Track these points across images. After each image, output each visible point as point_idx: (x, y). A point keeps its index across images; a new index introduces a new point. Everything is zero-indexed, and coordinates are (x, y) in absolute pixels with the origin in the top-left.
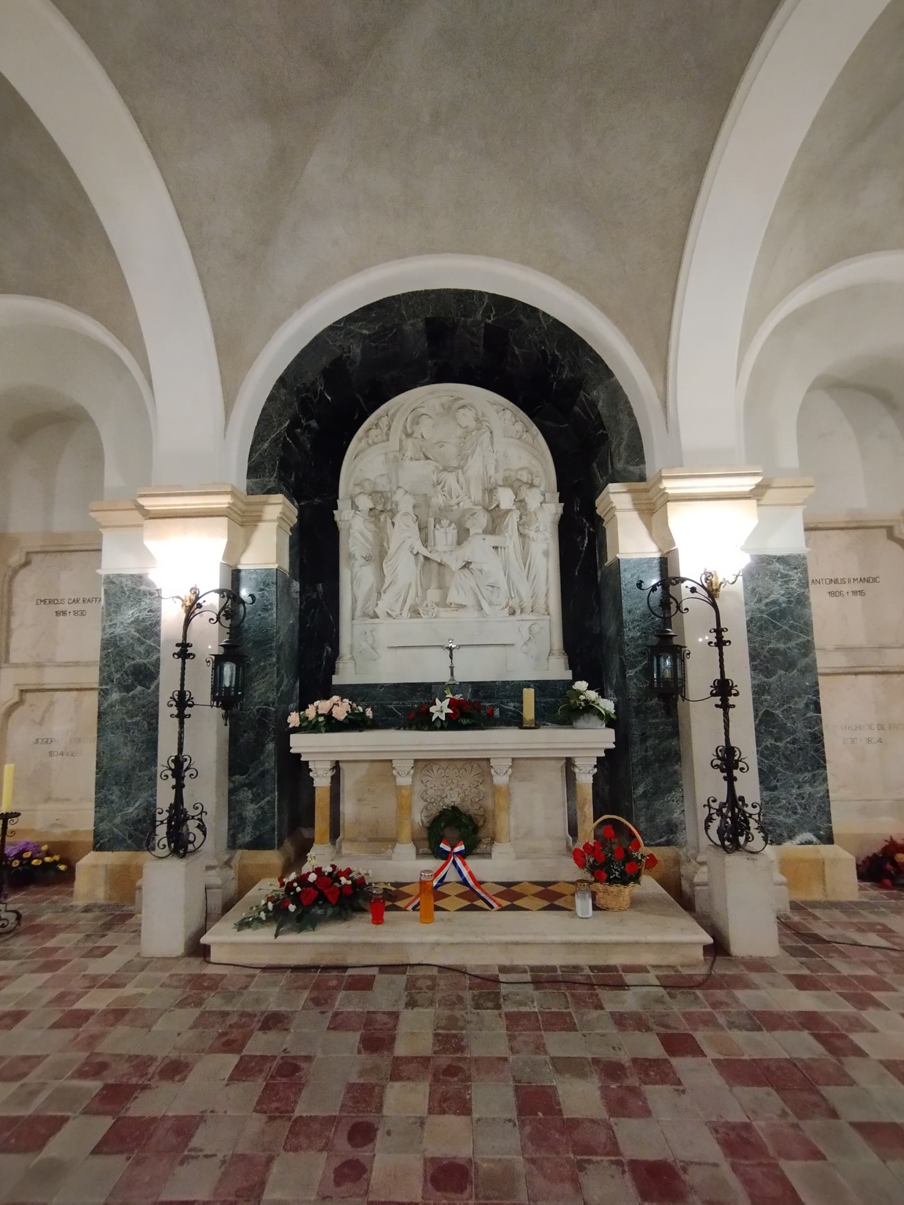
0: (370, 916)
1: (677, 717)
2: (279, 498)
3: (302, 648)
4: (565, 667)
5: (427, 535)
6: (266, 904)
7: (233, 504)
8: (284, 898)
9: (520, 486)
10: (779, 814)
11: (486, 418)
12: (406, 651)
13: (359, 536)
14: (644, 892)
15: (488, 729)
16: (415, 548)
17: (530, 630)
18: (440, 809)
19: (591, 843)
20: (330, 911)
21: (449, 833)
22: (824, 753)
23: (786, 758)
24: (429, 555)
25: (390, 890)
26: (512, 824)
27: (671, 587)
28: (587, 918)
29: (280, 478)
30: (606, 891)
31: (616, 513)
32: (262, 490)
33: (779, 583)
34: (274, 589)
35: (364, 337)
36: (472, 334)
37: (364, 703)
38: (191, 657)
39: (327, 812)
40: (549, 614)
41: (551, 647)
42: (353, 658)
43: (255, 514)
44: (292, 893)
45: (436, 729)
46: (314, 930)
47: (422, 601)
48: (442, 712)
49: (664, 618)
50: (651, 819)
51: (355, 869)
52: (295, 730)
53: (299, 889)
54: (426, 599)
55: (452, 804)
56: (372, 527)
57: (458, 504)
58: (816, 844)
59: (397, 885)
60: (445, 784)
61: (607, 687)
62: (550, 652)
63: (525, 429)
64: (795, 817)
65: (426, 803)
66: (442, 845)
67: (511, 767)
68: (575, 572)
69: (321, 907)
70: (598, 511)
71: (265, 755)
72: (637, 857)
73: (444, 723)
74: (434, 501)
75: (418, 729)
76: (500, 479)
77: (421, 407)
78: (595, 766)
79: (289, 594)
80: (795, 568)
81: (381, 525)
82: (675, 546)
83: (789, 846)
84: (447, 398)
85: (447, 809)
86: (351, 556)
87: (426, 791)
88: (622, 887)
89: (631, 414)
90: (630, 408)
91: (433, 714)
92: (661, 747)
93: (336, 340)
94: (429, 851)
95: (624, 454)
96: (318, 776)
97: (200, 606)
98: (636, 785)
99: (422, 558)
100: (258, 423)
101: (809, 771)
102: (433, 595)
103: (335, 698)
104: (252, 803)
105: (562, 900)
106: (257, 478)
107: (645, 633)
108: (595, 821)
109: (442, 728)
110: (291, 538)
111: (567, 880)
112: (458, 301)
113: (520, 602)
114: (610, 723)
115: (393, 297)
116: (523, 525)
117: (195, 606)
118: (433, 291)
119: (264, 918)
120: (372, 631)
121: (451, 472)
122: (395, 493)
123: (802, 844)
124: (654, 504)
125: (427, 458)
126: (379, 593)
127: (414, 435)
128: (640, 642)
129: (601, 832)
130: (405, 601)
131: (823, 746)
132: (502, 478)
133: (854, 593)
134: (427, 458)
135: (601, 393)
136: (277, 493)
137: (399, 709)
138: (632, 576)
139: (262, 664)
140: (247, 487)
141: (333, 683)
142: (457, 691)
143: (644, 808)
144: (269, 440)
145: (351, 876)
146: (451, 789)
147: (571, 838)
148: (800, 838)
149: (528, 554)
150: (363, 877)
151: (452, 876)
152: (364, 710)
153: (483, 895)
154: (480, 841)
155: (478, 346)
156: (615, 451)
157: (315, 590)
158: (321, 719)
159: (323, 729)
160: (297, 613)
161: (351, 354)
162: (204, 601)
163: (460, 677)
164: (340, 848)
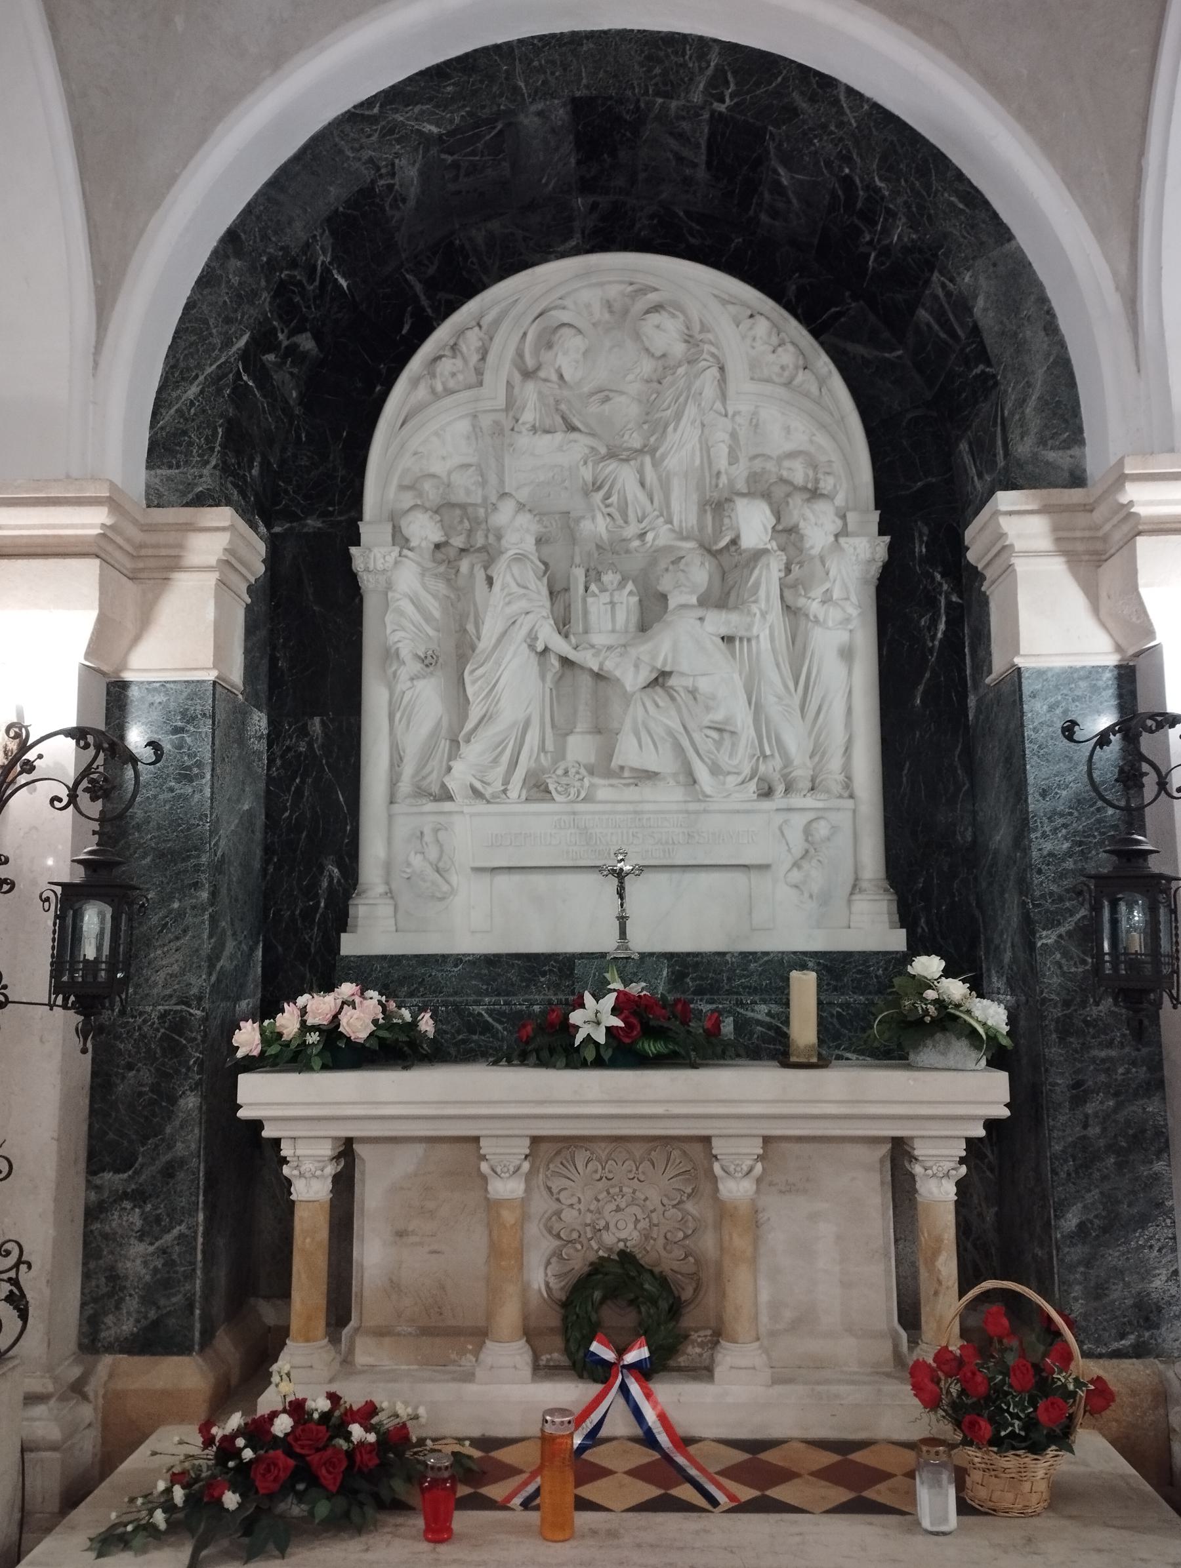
0: (420, 1522)
1: (1159, 1045)
2: (224, 515)
3: (271, 869)
4: (891, 922)
5: (568, 608)
6: (168, 1491)
7: (112, 527)
8: (213, 1476)
9: (788, 495)
11: (710, 336)
12: (516, 878)
13: (409, 609)
14: (1081, 1469)
15: (706, 1066)
16: (541, 636)
17: (807, 831)
18: (592, 1257)
19: (955, 1348)
20: (323, 1509)
21: (613, 1316)
24: (572, 655)
25: (469, 1457)
26: (764, 1297)
27: (1145, 738)
28: (944, 1534)
29: (225, 469)
30: (989, 1469)
31: (1013, 560)
32: (184, 494)
34: (206, 728)
35: (427, 141)
36: (681, 137)
37: (415, 1000)
38: (6, 887)
39: (321, 1262)
40: (851, 796)
41: (856, 873)
43: (164, 552)
44: (231, 1464)
45: (584, 1065)
46: (283, 1558)
47: (555, 762)
48: (598, 1023)
49: (1127, 809)
50: (1098, 1292)
51: (385, 1405)
52: (251, 1064)
53: (248, 1454)
54: (563, 758)
55: (621, 1245)
56: (441, 587)
57: (642, 536)
59: (487, 1443)
60: (603, 1196)
61: (989, 970)
62: (854, 886)
63: (801, 362)
65: (558, 1243)
66: (595, 1347)
67: (760, 1158)
68: (915, 698)
69: (300, 1497)
70: (971, 556)
71: (177, 1123)
72: (1064, 1386)
73: (602, 1051)
74: (586, 526)
75: (543, 1064)
76: (740, 472)
77: (555, 308)
78: (962, 1161)
79: (241, 741)
81: (461, 582)
82: (1154, 639)
84: (621, 287)
85: (608, 1259)
86: (390, 655)
87: (558, 1213)
88: (1028, 1459)
89: (1051, 327)
90: (1050, 313)
91: (577, 1028)
92: (1120, 1117)
93: (362, 147)
94: (564, 1360)
95: (1035, 424)
96: (301, 1175)
97: (29, 767)
98: (1061, 1208)
99: (555, 663)
100: (174, 338)
102: (580, 747)
103: (347, 989)
104: (141, 1239)
105: (881, 1487)
106: (170, 467)
107: (1080, 843)
108: (962, 1293)
109: (599, 1063)
110: (249, 609)
111: (896, 1437)
112: (649, 58)
113: (785, 767)
114: (999, 1059)
115: (497, 48)
116: (794, 586)
117: (18, 768)
118: (591, 35)
119: (163, 1526)
121: (627, 460)
122: (495, 507)
124: (1105, 539)
125: (572, 428)
126: (455, 743)
127: (542, 374)
128: (1069, 864)
129: (973, 1321)
130: (514, 763)
132: (745, 474)
134: (572, 428)
135: (982, 280)
136: (217, 505)
137: (499, 1016)
138: (1051, 708)
139: (176, 905)
140: (148, 486)
141: (343, 952)
142: (635, 974)
143: (1079, 1263)
144: (201, 378)
145: (374, 1421)
146: (618, 1209)
147: (904, 1335)
149: (805, 648)
150: (404, 1426)
151: (619, 1424)
152: (414, 1016)
153: (693, 1472)
154: (687, 1337)
155: (695, 165)
156: (1012, 414)
157: (303, 732)
158: (313, 1038)
159: (317, 1062)
160: (262, 785)
161: (397, 180)
162: (40, 757)
163: (642, 941)
164: (351, 1350)
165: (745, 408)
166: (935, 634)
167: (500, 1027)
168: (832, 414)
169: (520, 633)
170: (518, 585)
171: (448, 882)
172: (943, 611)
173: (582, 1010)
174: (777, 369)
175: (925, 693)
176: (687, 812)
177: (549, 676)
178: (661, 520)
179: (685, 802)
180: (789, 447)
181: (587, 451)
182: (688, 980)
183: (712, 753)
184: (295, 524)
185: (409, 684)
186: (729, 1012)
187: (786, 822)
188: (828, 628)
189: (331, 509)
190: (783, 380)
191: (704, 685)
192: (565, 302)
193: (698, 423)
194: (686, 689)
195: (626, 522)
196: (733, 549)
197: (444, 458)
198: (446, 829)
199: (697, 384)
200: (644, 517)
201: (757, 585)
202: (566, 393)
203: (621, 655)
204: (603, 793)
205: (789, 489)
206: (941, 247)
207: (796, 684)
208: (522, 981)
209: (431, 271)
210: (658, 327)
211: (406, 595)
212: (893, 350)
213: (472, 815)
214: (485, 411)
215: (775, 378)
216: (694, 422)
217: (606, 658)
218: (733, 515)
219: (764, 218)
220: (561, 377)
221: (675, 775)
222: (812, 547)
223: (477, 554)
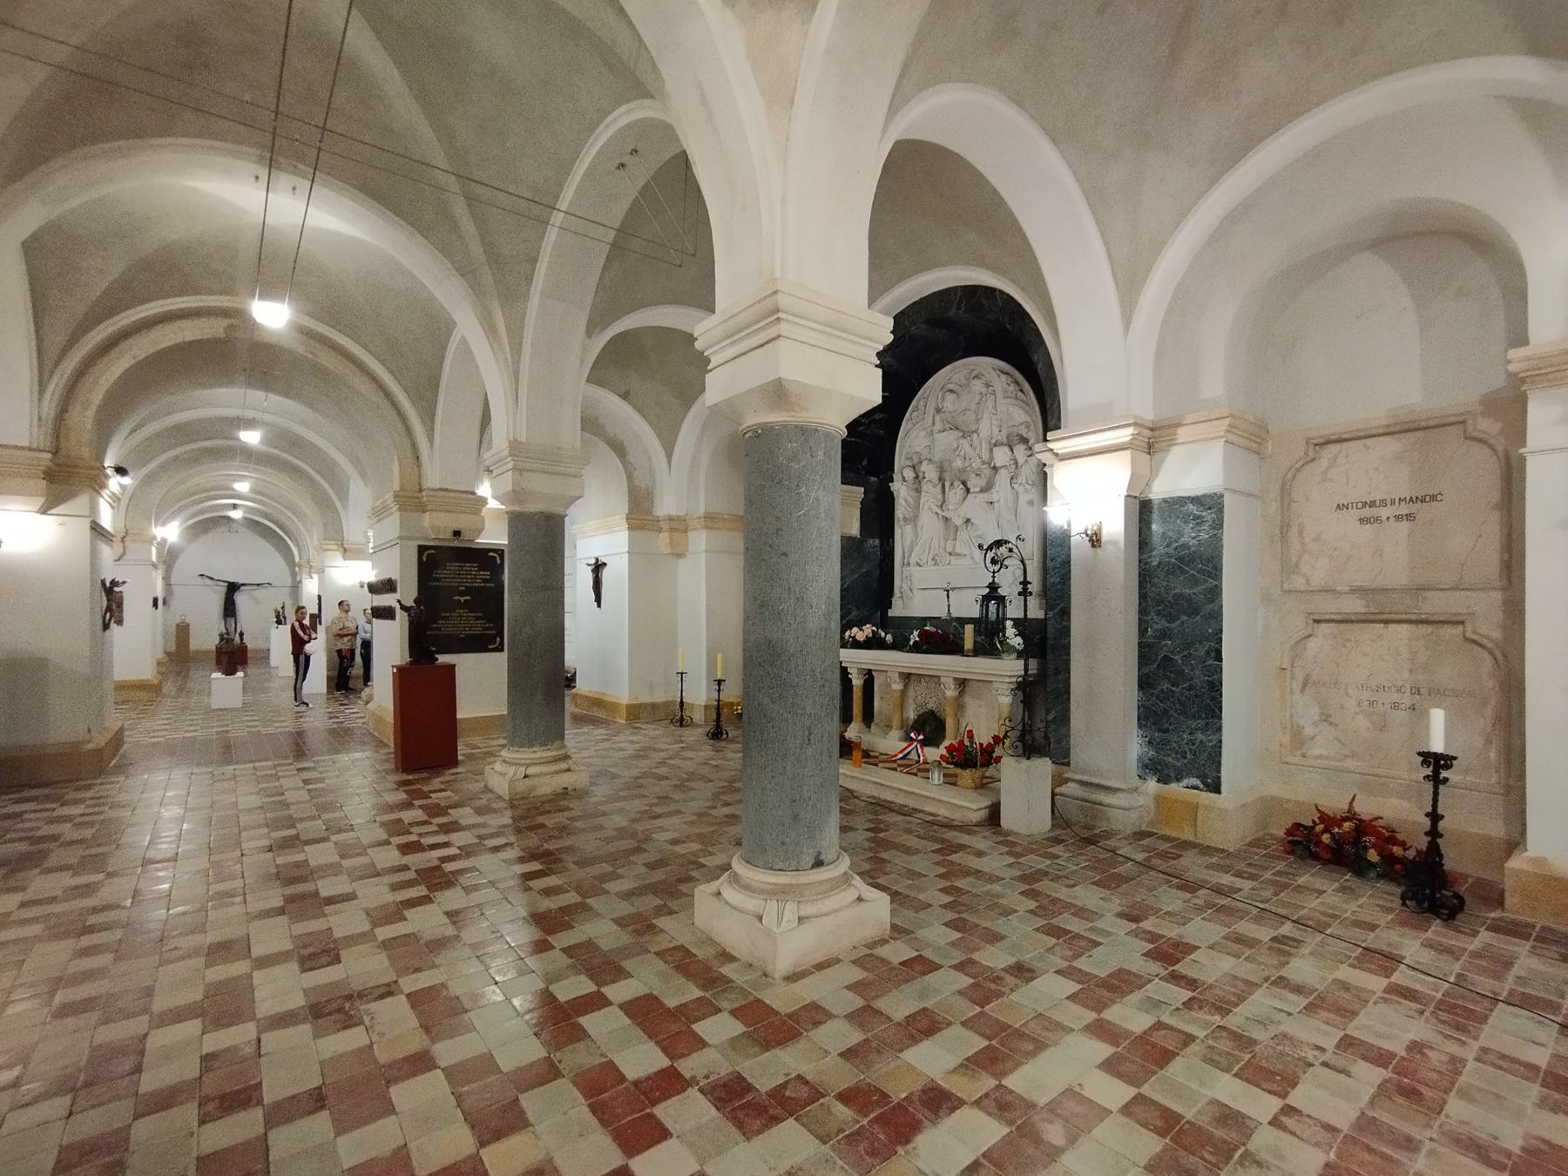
10: (1169, 755)
22: (1221, 702)
23: (1182, 704)
33: (1191, 525)
58: (1201, 790)
64: (1186, 761)
80: (1210, 509)
83: (1175, 788)
101: (1202, 719)
123: (1188, 787)
131: (1221, 696)
133: (1399, 518)
148: (1185, 782)
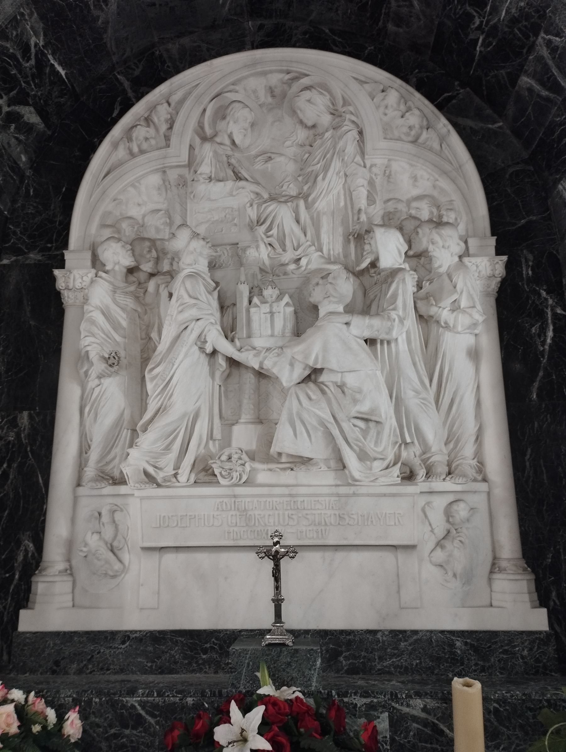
4: (531, 601)
11: (351, 108)
12: (182, 556)
17: (448, 513)
24: (237, 356)
40: (485, 480)
41: (494, 551)
42: (70, 571)
47: (222, 448)
54: (229, 445)
56: (130, 303)
62: (493, 564)
63: (425, 123)
74: (252, 253)
81: (149, 299)
84: (280, 76)
99: (222, 362)
113: (424, 453)
116: (426, 298)
120: (113, 512)
121: (286, 202)
126: (134, 433)
132: (381, 213)
134: (238, 177)
137: (152, 709)
141: (22, 627)
157: (13, 424)
165: (380, 161)
166: (545, 341)
167: (152, 721)
168: (451, 163)
169: (191, 336)
170: (190, 296)
171: (120, 561)
172: (550, 321)
173: (227, 725)
174: (405, 130)
175: (540, 389)
176: (338, 495)
177: (218, 374)
178: (313, 248)
179: (337, 486)
180: (415, 192)
181: (253, 196)
182: (341, 659)
183: (360, 441)
184: (20, 258)
185: (97, 382)
186: (384, 707)
187: (428, 503)
188: (459, 333)
189: (49, 245)
190: (410, 139)
191: (351, 380)
192: (237, 88)
193: (342, 173)
194: (335, 383)
195: (284, 250)
196: (372, 271)
197: (139, 205)
198: (122, 510)
199: (341, 144)
200: (299, 246)
201: (395, 297)
202: (237, 155)
203: (279, 355)
204: (262, 477)
205: (417, 223)
206: (548, 6)
207: (431, 381)
208: (184, 658)
209: (137, 72)
210: (309, 101)
211: (97, 308)
212: (494, 122)
213: (142, 498)
214: (171, 167)
215: (403, 137)
216: (338, 173)
217: (265, 358)
218: (372, 242)
219: (391, 27)
220: (233, 143)
221: (326, 460)
222: (440, 267)
223: (162, 277)
